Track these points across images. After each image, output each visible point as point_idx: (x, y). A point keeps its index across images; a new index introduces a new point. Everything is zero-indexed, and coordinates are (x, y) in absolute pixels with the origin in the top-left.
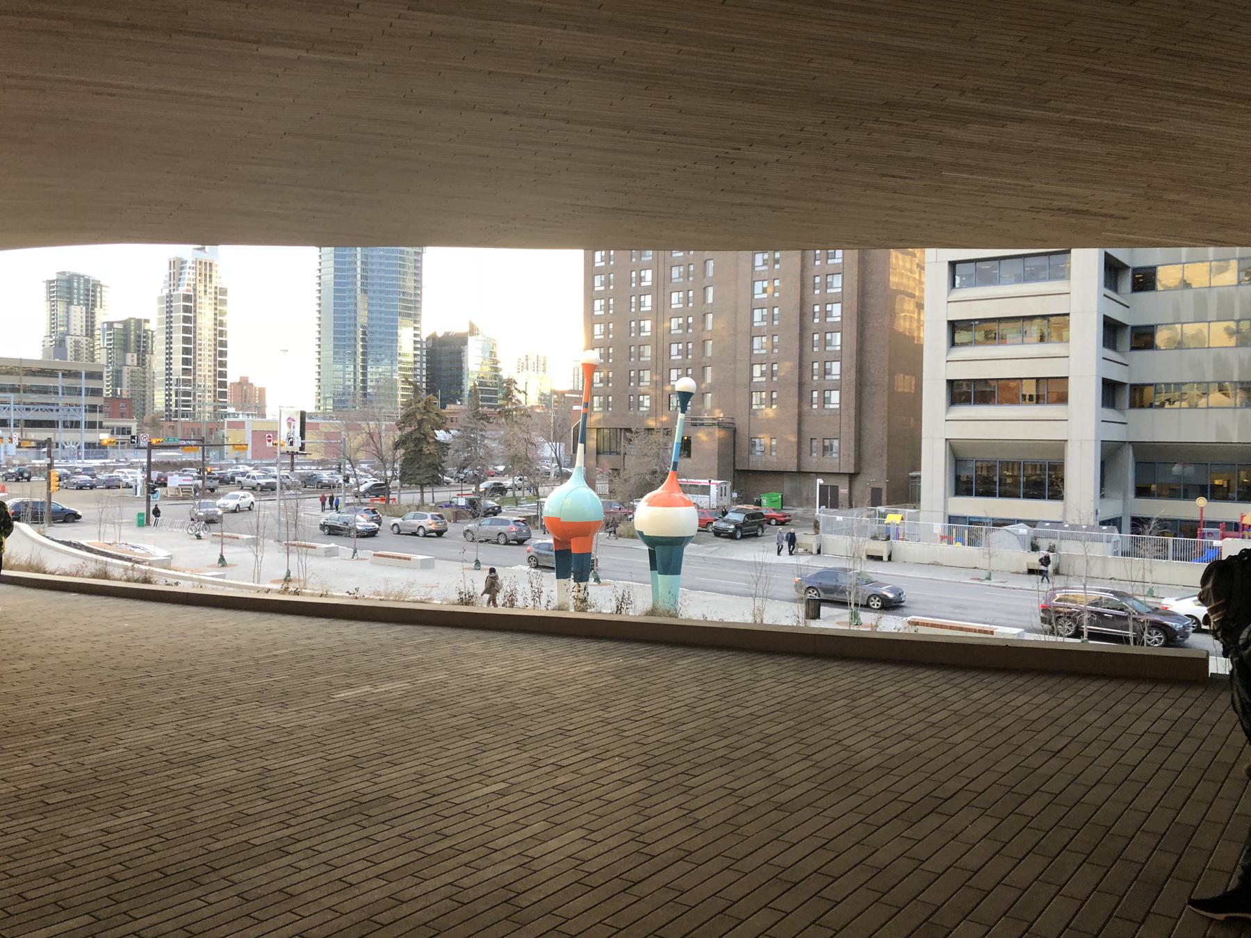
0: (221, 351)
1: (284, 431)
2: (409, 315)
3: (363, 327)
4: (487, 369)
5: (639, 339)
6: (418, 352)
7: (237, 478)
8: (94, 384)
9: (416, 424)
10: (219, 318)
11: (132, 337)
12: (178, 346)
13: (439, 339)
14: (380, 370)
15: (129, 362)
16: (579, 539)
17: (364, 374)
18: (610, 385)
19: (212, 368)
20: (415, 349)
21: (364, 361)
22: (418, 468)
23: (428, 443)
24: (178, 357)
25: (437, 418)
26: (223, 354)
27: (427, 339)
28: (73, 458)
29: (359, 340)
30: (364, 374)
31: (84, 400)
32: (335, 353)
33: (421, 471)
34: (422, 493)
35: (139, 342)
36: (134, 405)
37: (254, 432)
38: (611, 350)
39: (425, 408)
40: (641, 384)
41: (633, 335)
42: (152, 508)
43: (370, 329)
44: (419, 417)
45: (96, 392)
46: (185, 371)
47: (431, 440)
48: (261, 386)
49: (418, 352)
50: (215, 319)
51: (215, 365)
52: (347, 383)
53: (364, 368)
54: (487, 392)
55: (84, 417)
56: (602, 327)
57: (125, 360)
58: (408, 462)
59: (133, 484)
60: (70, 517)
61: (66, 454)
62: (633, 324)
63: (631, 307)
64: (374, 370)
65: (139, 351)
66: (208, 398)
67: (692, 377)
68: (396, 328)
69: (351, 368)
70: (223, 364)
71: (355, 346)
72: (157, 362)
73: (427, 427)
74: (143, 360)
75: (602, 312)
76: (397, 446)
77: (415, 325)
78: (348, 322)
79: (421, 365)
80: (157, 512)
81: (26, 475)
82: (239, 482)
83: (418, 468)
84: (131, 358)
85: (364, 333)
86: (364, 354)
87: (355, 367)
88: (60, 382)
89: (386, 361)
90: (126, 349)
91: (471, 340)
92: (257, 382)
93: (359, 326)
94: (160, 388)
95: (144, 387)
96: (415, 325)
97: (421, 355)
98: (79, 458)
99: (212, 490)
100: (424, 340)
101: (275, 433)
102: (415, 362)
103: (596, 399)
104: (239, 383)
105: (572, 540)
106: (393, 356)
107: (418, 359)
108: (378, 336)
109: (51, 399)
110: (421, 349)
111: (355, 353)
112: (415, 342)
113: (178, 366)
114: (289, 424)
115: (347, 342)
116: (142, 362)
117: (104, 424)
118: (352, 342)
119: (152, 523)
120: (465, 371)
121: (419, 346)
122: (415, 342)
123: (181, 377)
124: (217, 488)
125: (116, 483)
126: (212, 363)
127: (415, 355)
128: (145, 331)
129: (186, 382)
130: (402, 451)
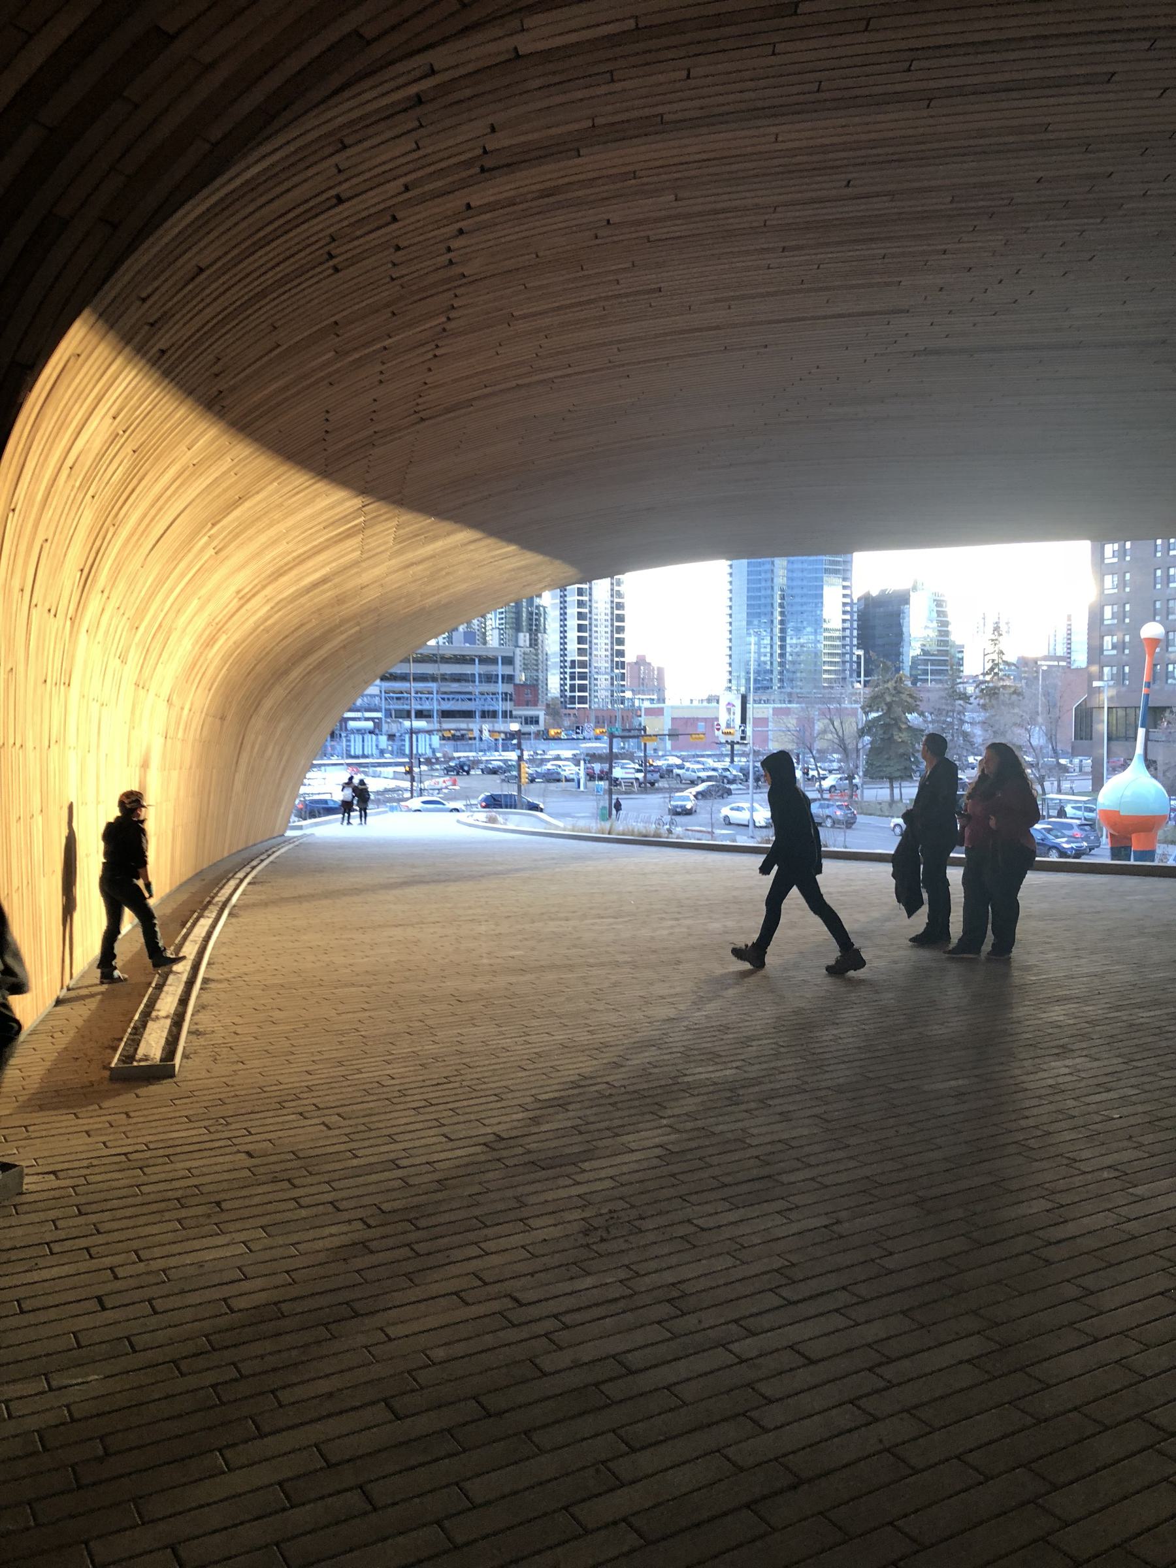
0: (618, 627)
1: (723, 720)
2: (836, 572)
3: (782, 590)
4: (933, 634)
5: (1168, 591)
6: (848, 617)
7: (676, 771)
8: (508, 670)
9: (885, 707)
10: (616, 588)
11: (524, 615)
12: (573, 623)
13: (873, 598)
14: (802, 641)
15: (521, 643)
16: (1142, 834)
17: (783, 647)
18: (1127, 651)
19: (609, 647)
20: (844, 613)
21: (783, 631)
22: (888, 759)
23: (900, 729)
24: (573, 635)
25: (910, 700)
26: (620, 630)
27: (859, 599)
28: (489, 749)
29: (776, 605)
30: (783, 647)
31: (501, 687)
32: (749, 623)
33: (891, 763)
34: (892, 788)
35: (531, 619)
36: (530, 692)
37: (673, 719)
38: (1128, 607)
39: (895, 688)
40: (1170, 649)
41: (1158, 586)
42: (614, 801)
43: (790, 592)
44: (888, 699)
45: (509, 679)
46: (581, 652)
47: (903, 726)
48: (661, 666)
49: (848, 617)
50: (612, 590)
51: (612, 643)
52: (763, 659)
53: (783, 639)
54: (933, 662)
55: (500, 706)
56: (1116, 579)
57: (517, 641)
58: (874, 752)
59: (575, 777)
60: (535, 807)
61: (484, 746)
62: (1159, 573)
63: (1156, 551)
64: (794, 641)
65: (531, 630)
66: (603, 681)
67: (1160, 622)
68: (822, 588)
69: (767, 641)
70: (621, 642)
71: (772, 613)
72: (551, 642)
73: (898, 710)
74: (536, 640)
75: (1115, 560)
76: (862, 733)
77: (845, 584)
78: (763, 584)
79: (851, 633)
80: (618, 807)
81: (466, 768)
82: (678, 775)
83: (888, 759)
84: (524, 638)
85: (783, 597)
86: (782, 622)
87: (772, 638)
88: (477, 669)
89: (809, 629)
90: (518, 629)
91: (914, 598)
92: (655, 661)
93: (776, 588)
94: (554, 671)
95: (537, 670)
96: (845, 584)
97: (852, 621)
98: (496, 750)
99: (652, 784)
100: (855, 601)
101: (717, 719)
102: (844, 629)
103: (1106, 670)
104: (636, 663)
105: (1134, 836)
106: (818, 621)
107: (847, 625)
108: (798, 600)
109: (469, 687)
110: (851, 613)
111: (772, 622)
112: (845, 604)
113: (573, 646)
114: (729, 710)
115: (763, 610)
116: (534, 643)
117: (514, 713)
118: (769, 609)
119: (614, 816)
120: (905, 636)
121: (848, 608)
122: (845, 604)
123: (577, 658)
124: (656, 781)
125: (557, 777)
126: (609, 641)
127: (844, 621)
128: (538, 607)
129: (583, 664)
130: (867, 739)
